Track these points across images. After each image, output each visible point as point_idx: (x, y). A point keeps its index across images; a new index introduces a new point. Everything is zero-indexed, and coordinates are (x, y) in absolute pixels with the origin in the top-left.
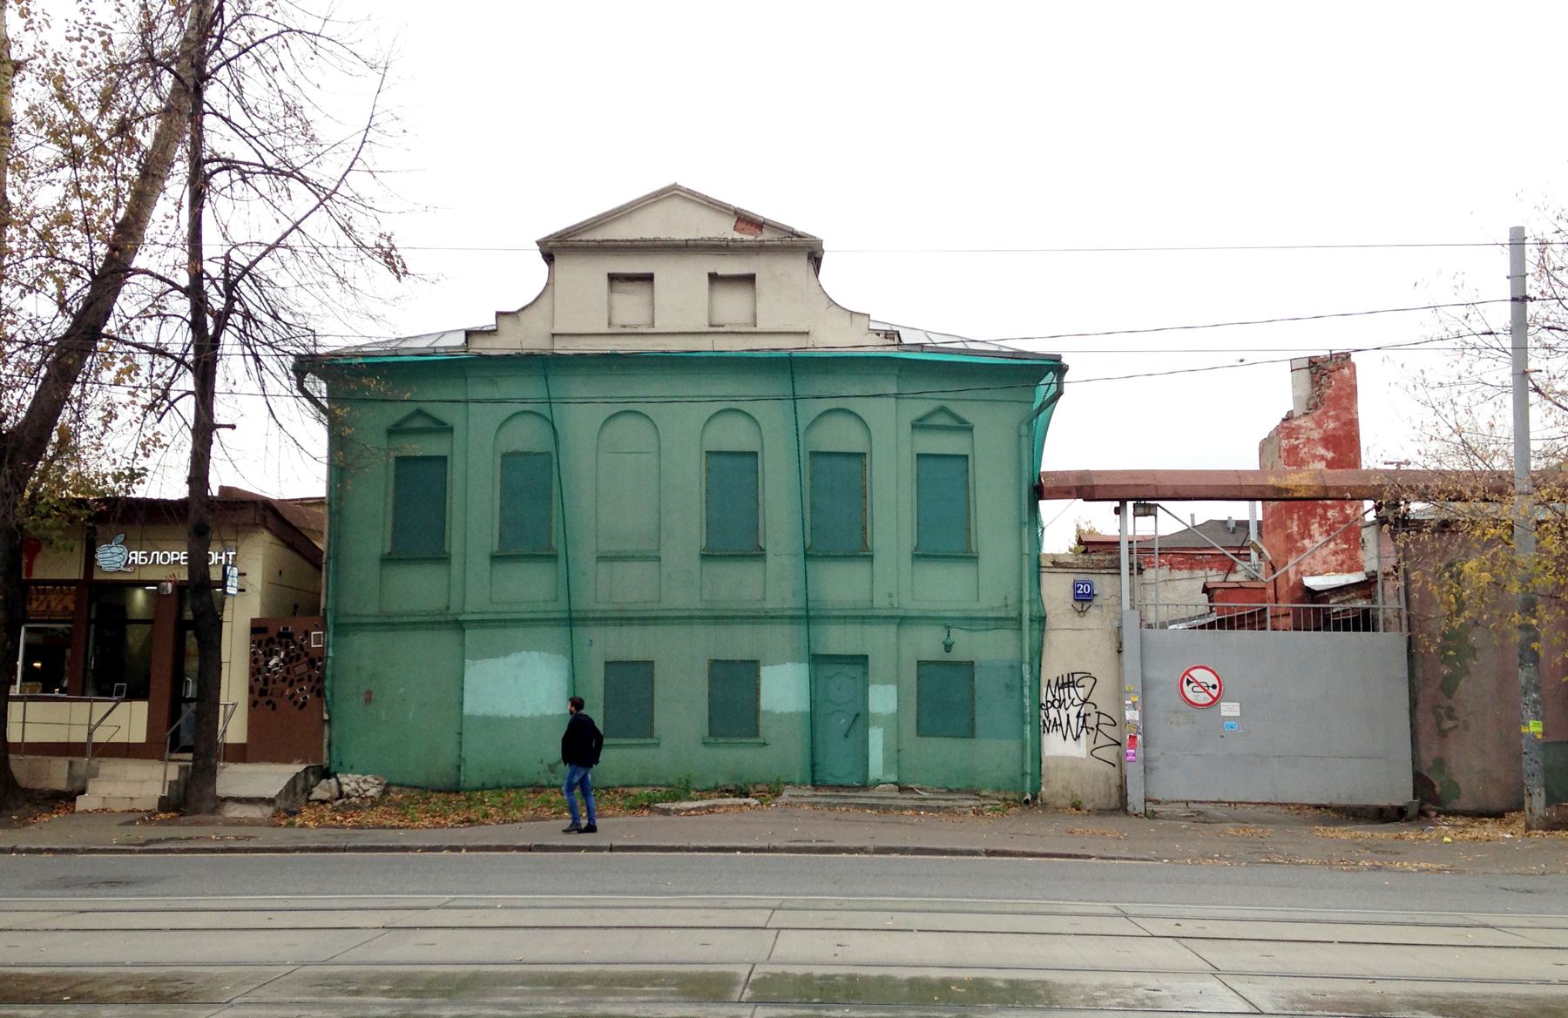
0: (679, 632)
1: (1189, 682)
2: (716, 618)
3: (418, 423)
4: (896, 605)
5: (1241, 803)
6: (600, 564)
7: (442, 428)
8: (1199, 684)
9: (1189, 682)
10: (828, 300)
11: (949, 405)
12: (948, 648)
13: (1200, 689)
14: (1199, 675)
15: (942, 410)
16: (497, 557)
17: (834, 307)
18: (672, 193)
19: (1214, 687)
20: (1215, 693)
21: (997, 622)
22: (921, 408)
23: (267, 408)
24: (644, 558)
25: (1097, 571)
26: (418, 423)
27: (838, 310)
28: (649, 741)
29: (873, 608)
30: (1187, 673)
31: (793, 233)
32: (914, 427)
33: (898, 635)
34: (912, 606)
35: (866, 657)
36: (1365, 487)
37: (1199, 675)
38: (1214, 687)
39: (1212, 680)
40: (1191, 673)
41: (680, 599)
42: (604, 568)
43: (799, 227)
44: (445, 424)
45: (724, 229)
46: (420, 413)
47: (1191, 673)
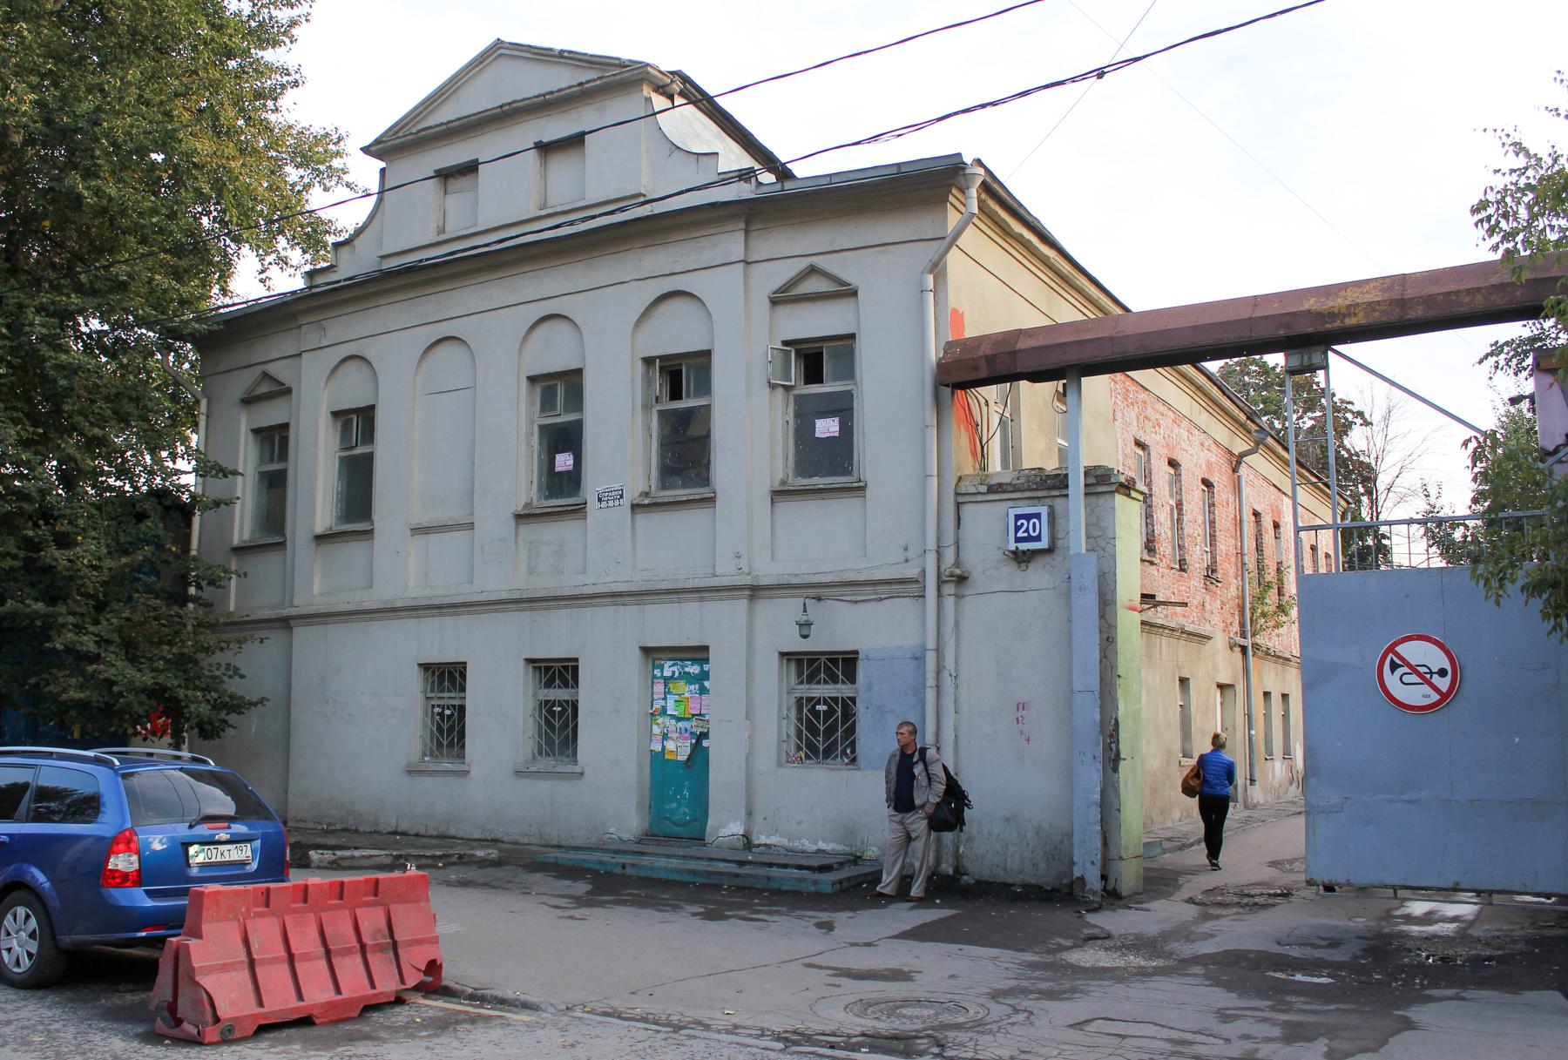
0: (604, 615)
1: (1394, 667)
2: (530, 600)
3: (814, 285)
4: (746, 570)
5: (1499, 892)
6: (640, 518)
7: (284, 391)
8: (1414, 670)
9: (1394, 667)
10: (670, 145)
11: (820, 262)
12: (805, 627)
13: (1415, 678)
14: (1413, 652)
15: (813, 271)
16: (637, 505)
17: (677, 152)
18: (499, 51)
19: (1442, 673)
20: (1443, 684)
21: (903, 587)
22: (778, 275)
23: (289, 360)
24: (458, 527)
25: (1044, 493)
26: (814, 285)
27: (683, 155)
28: (570, 768)
29: (714, 575)
30: (1391, 649)
31: (621, 64)
32: (774, 302)
33: (751, 612)
34: (767, 572)
35: (706, 649)
36: (1479, 289)
37: (1413, 652)
38: (1442, 673)
39: (1438, 660)
40: (1398, 649)
41: (492, 584)
42: (416, 544)
43: (626, 54)
44: (284, 385)
45: (562, 79)
46: (813, 271)
47: (1398, 649)
